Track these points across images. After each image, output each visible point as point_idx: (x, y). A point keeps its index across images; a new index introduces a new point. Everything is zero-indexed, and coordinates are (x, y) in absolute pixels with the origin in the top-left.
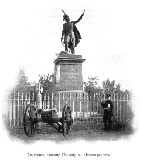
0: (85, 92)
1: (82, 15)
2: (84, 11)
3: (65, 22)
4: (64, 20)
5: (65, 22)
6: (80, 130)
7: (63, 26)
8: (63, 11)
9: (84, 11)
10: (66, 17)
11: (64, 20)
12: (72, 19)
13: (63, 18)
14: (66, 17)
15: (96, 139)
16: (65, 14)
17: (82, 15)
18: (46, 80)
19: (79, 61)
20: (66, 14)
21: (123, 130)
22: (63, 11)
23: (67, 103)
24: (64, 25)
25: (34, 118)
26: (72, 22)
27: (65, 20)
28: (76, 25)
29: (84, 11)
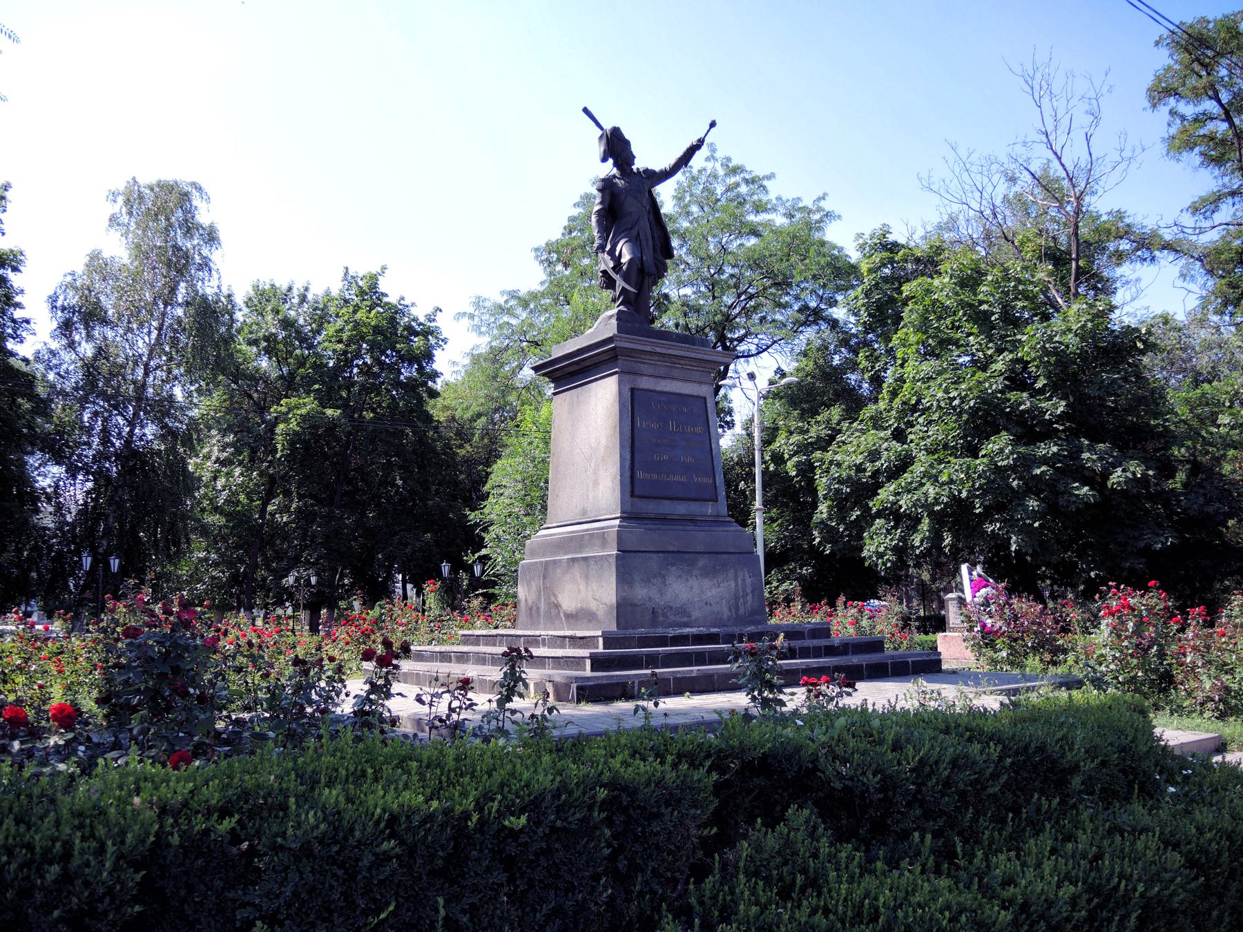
5: (608, 169)
8: (586, 110)
9: (713, 124)
11: (604, 160)
14: (770, 177)
22: (586, 110)
27: (611, 161)
29: (713, 124)
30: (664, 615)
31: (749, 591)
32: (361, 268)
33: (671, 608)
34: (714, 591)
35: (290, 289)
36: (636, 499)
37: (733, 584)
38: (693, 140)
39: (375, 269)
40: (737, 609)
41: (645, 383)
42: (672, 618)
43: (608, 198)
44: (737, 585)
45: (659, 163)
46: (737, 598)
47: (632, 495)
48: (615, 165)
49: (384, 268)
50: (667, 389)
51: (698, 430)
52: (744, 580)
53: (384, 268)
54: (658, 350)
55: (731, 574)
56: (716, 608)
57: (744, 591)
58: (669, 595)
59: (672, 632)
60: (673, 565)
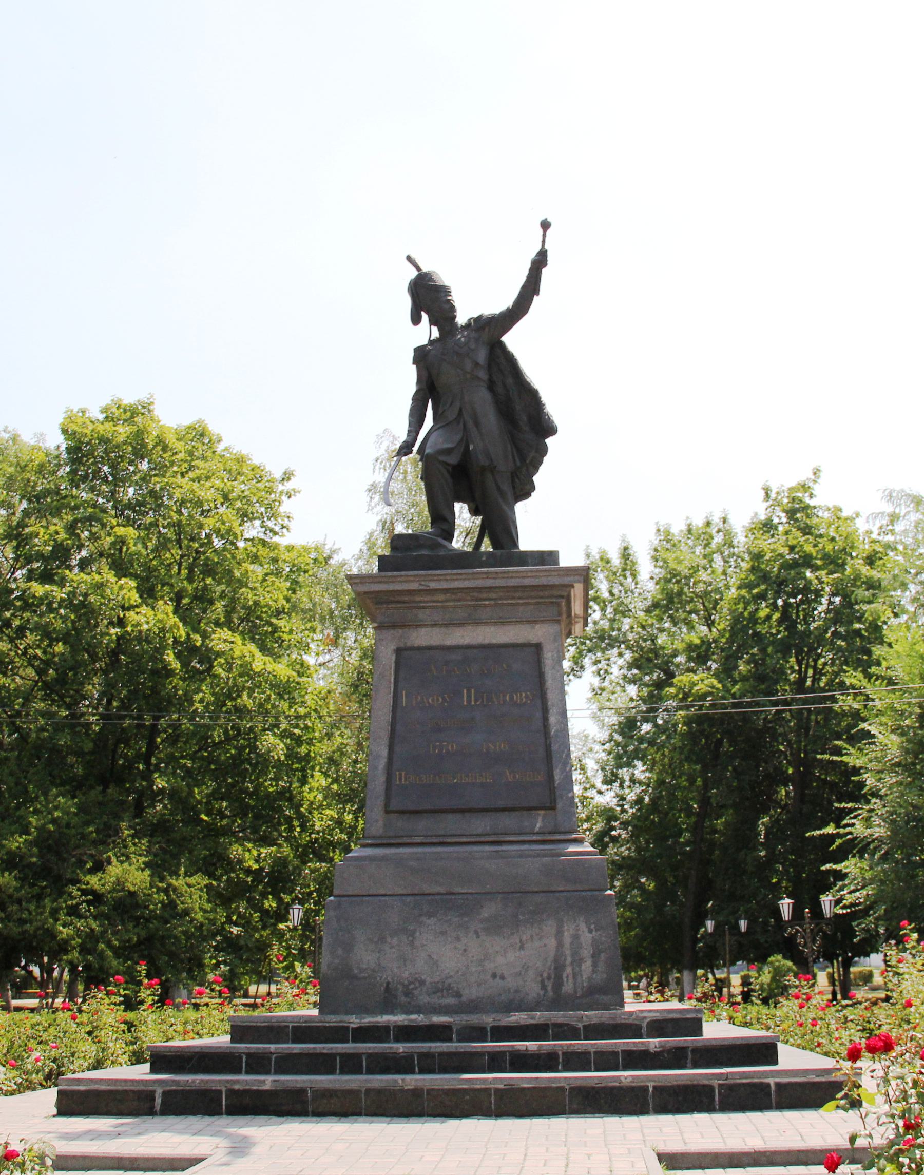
0: (858, 763)
1: (540, 261)
2: (541, 231)
3: (425, 332)
4: (416, 320)
5: (425, 332)
7: (415, 367)
8: (409, 258)
9: (545, 225)
10: (428, 297)
11: (416, 320)
13: (407, 302)
14: (428, 297)
16: (418, 269)
17: (540, 261)
18: (766, 986)
22: (409, 258)
23: (852, 732)
24: (421, 356)
25: (873, 649)
27: (425, 317)
28: (512, 340)
29: (545, 225)
30: (407, 994)
31: (586, 952)
32: (785, 480)
33: (422, 983)
34: (512, 956)
35: (708, 524)
36: (393, 816)
37: (552, 943)
38: (533, 254)
39: (805, 475)
40: (558, 984)
41: (423, 637)
42: (424, 999)
43: (425, 374)
44: (560, 945)
45: (499, 301)
46: (559, 968)
47: (387, 812)
48: (432, 322)
49: (816, 472)
50: (466, 641)
51: (522, 697)
52: (576, 937)
53: (816, 472)
54: (433, 585)
55: (550, 927)
56: (511, 983)
57: (575, 954)
58: (419, 966)
59: (354, 1021)
60: (430, 915)
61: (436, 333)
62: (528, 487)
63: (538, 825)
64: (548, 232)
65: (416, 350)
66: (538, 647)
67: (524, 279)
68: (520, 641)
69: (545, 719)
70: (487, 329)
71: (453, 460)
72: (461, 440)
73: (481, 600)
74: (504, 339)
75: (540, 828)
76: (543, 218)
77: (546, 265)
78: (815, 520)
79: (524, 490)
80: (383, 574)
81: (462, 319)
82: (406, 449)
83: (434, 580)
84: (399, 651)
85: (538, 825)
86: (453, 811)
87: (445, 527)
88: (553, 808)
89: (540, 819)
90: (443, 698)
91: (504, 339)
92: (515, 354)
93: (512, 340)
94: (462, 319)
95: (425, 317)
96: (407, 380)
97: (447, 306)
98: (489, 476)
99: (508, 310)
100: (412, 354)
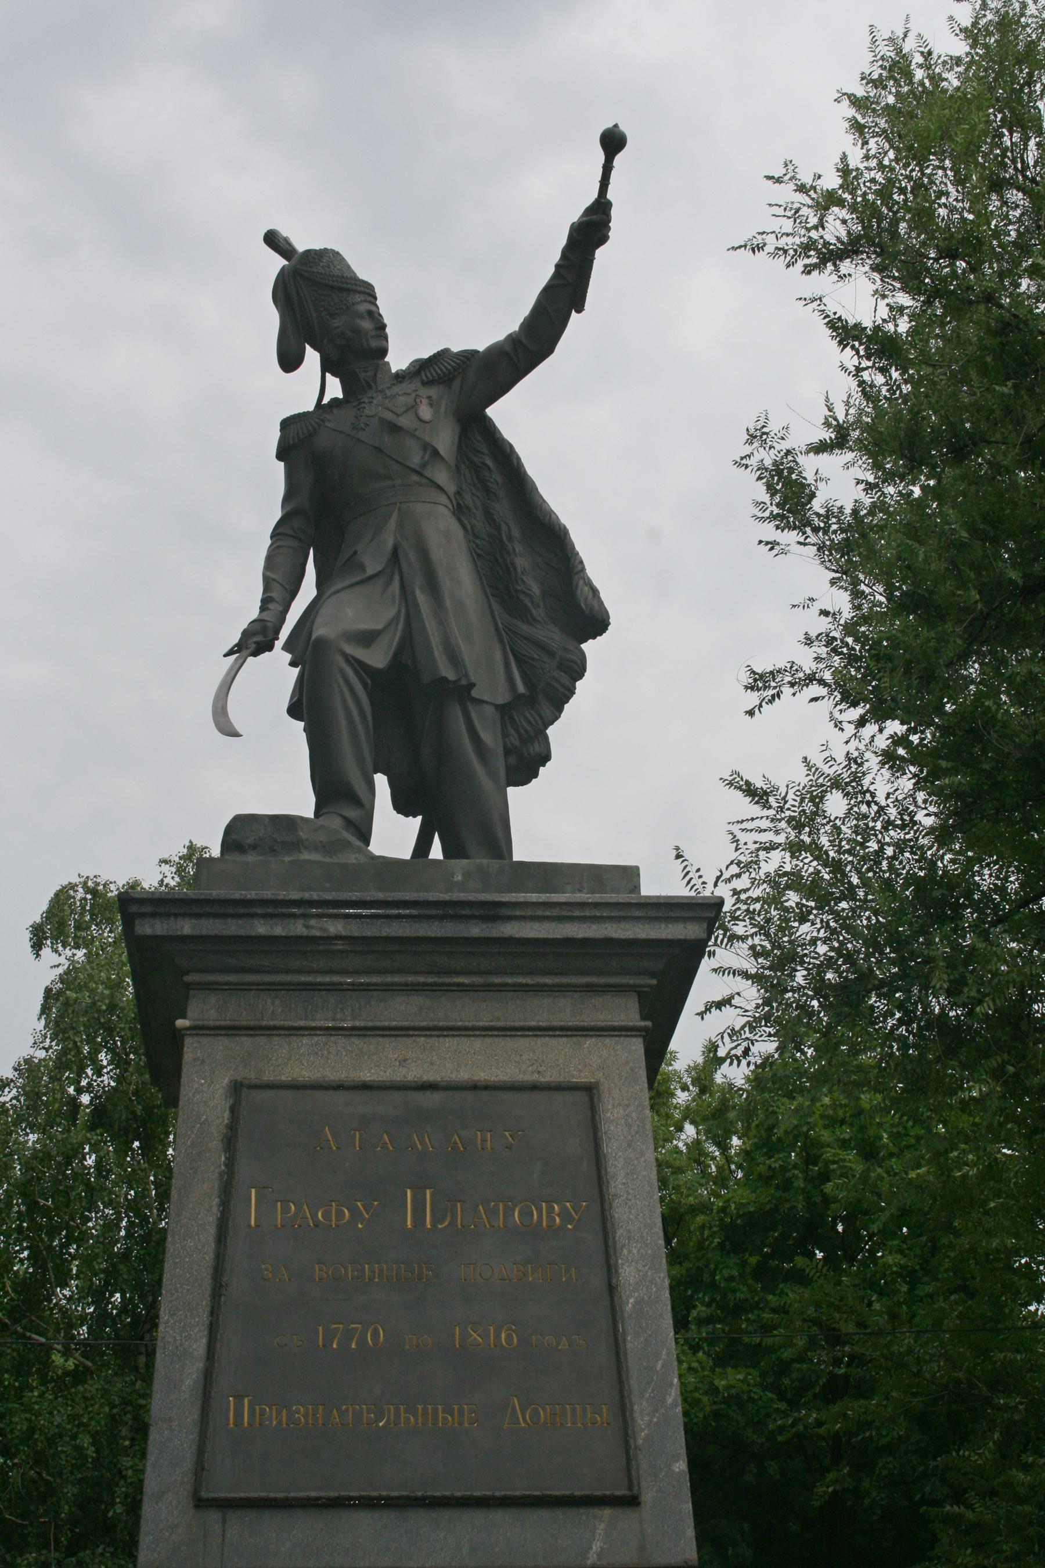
1: (591, 231)
2: (601, 157)
4: (289, 361)
5: (309, 386)
6: (636, 1488)
9: (613, 142)
11: (289, 361)
12: (428, 317)
13: (270, 320)
15: (504, 440)
17: (591, 231)
19: (341, 289)
20: (301, 245)
21: (693, 1331)
23: (253, 1223)
24: (298, 441)
26: (439, 370)
27: (312, 357)
28: (508, 414)
29: (613, 142)
45: (485, 324)
47: (201, 1503)
61: (335, 389)
62: (536, 748)
63: (596, 1546)
64: (619, 160)
65: (285, 424)
66: (590, 1090)
67: (548, 272)
68: (550, 1077)
69: (610, 1268)
70: (457, 383)
71: (378, 658)
72: (396, 618)
73: (450, 973)
74: (491, 411)
75: (600, 1554)
76: (610, 125)
77: (603, 239)
78: (765, 1321)
79: (527, 762)
80: (305, 716)
81: (399, 358)
82: (256, 641)
83: (336, 916)
84: (237, 1088)
85: (596, 1546)
86: (371, 1503)
87: (353, 813)
88: (632, 1501)
89: (601, 1528)
90: (354, 1211)
91: (491, 411)
92: (518, 449)
93: (508, 414)
94: (399, 358)
95: (312, 357)
96: (261, 494)
97: (367, 325)
98: (456, 715)
99: (512, 340)
100: (275, 435)
